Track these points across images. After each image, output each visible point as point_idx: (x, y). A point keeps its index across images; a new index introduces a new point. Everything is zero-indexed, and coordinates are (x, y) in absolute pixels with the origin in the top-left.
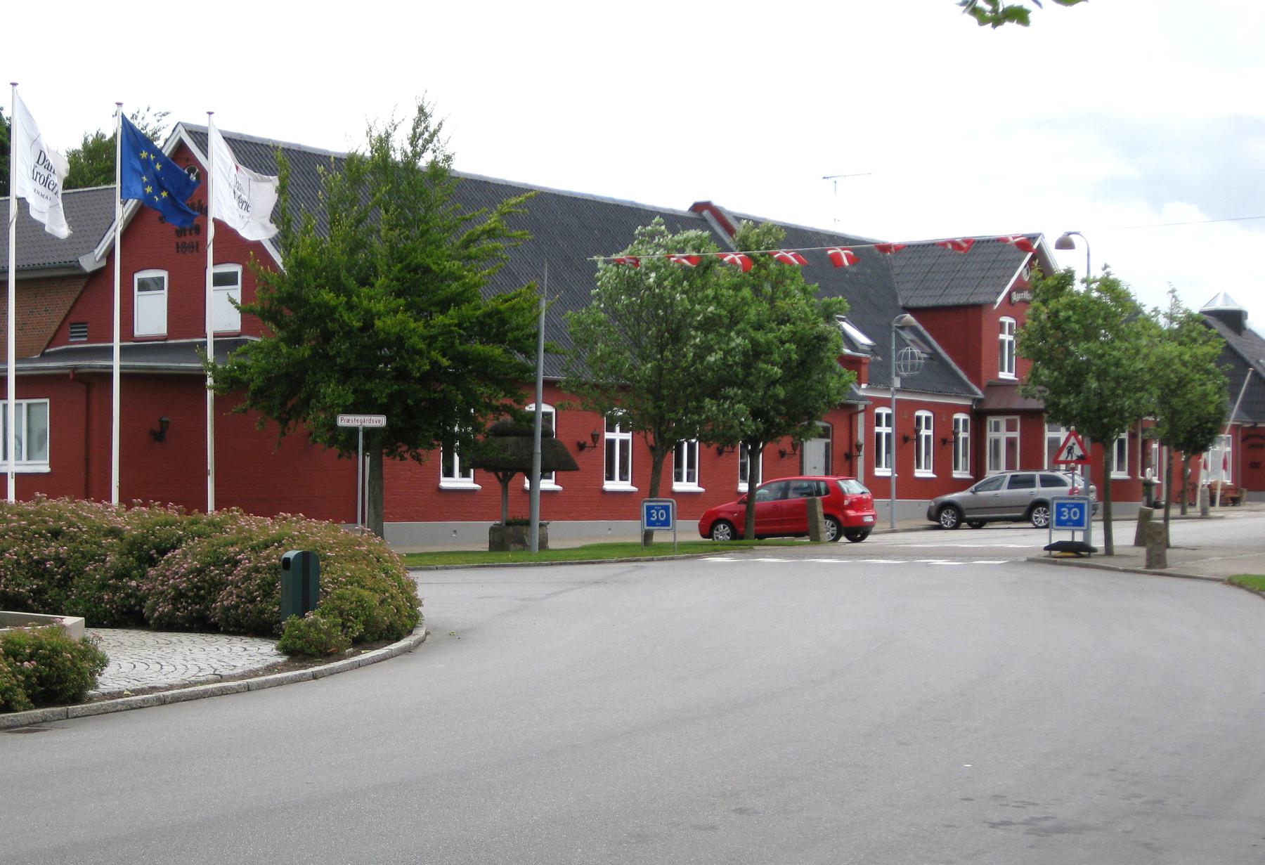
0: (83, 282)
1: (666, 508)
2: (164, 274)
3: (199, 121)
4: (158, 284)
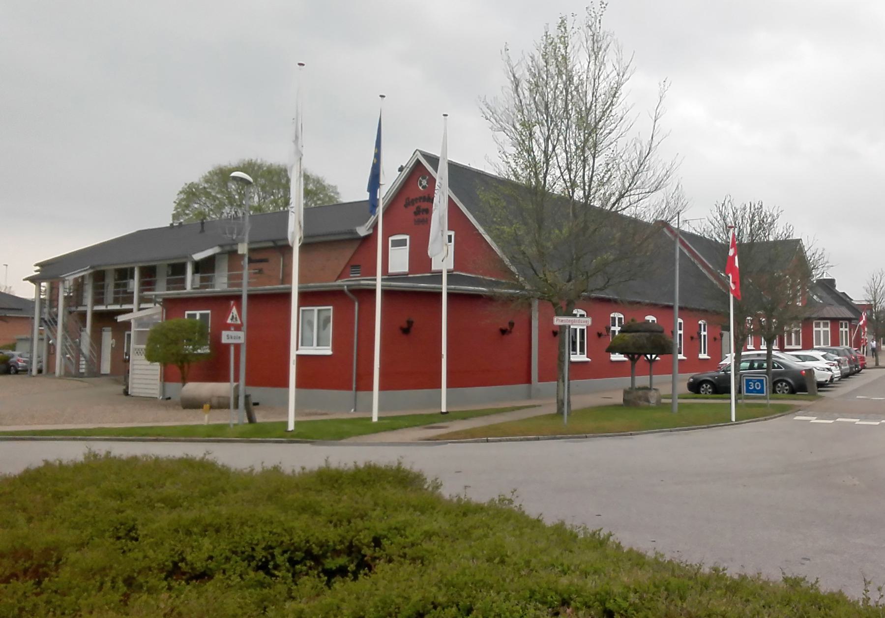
0: (356, 245)
1: (761, 381)
2: (407, 237)
3: (436, 152)
4: (402, 243)
